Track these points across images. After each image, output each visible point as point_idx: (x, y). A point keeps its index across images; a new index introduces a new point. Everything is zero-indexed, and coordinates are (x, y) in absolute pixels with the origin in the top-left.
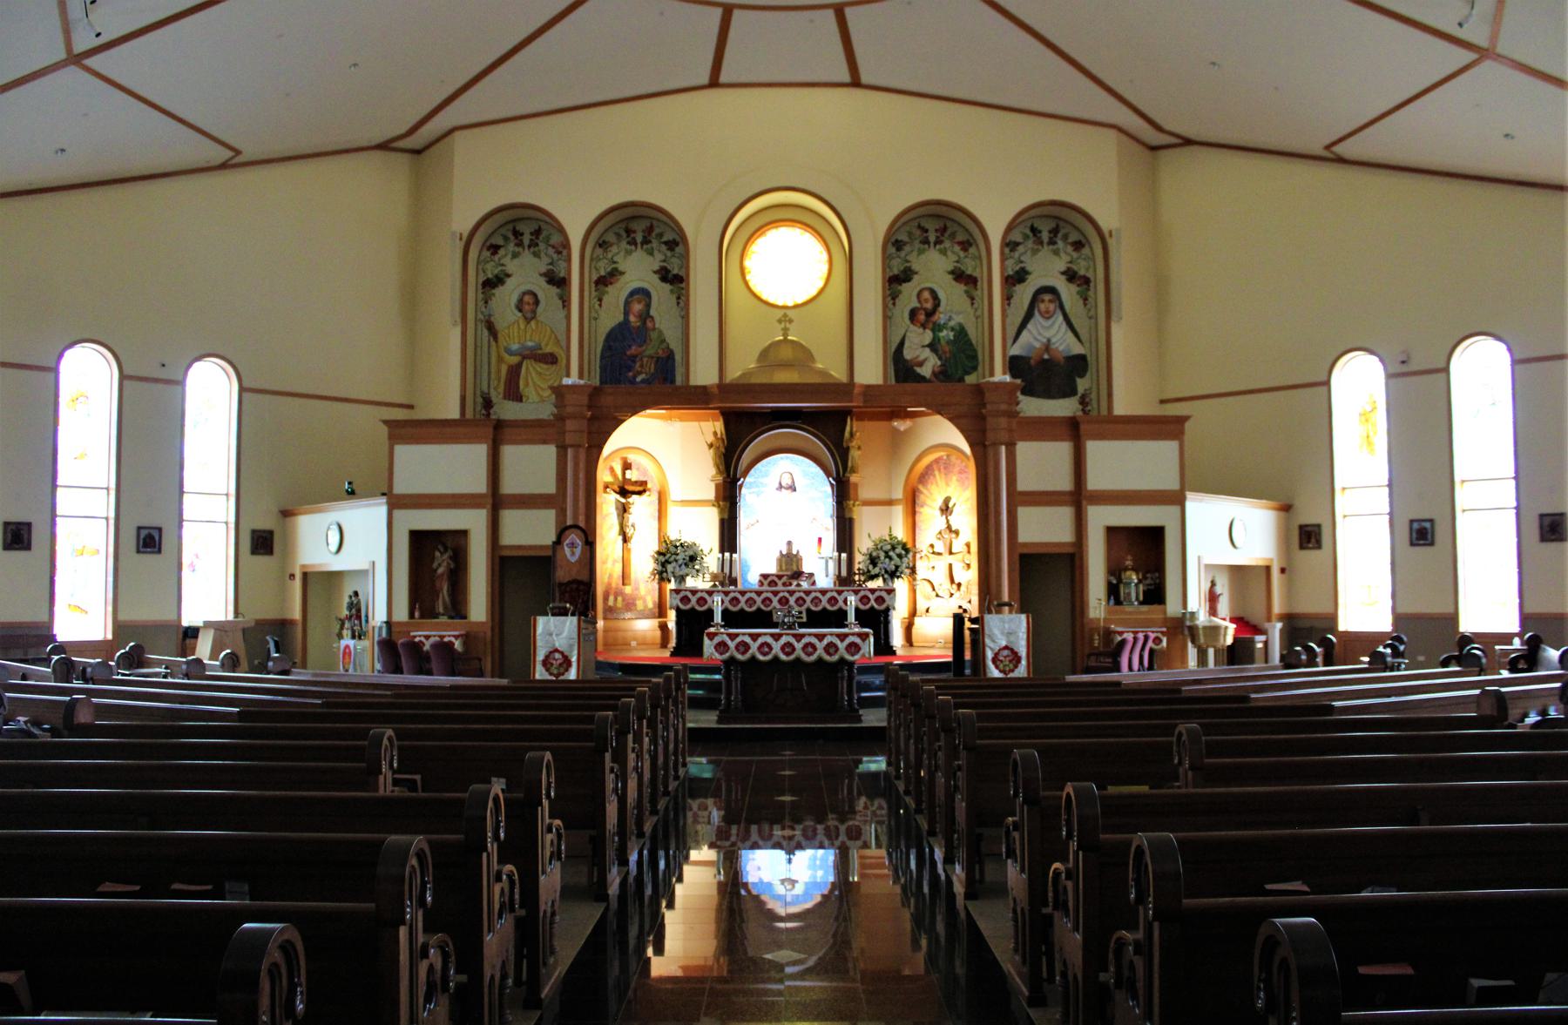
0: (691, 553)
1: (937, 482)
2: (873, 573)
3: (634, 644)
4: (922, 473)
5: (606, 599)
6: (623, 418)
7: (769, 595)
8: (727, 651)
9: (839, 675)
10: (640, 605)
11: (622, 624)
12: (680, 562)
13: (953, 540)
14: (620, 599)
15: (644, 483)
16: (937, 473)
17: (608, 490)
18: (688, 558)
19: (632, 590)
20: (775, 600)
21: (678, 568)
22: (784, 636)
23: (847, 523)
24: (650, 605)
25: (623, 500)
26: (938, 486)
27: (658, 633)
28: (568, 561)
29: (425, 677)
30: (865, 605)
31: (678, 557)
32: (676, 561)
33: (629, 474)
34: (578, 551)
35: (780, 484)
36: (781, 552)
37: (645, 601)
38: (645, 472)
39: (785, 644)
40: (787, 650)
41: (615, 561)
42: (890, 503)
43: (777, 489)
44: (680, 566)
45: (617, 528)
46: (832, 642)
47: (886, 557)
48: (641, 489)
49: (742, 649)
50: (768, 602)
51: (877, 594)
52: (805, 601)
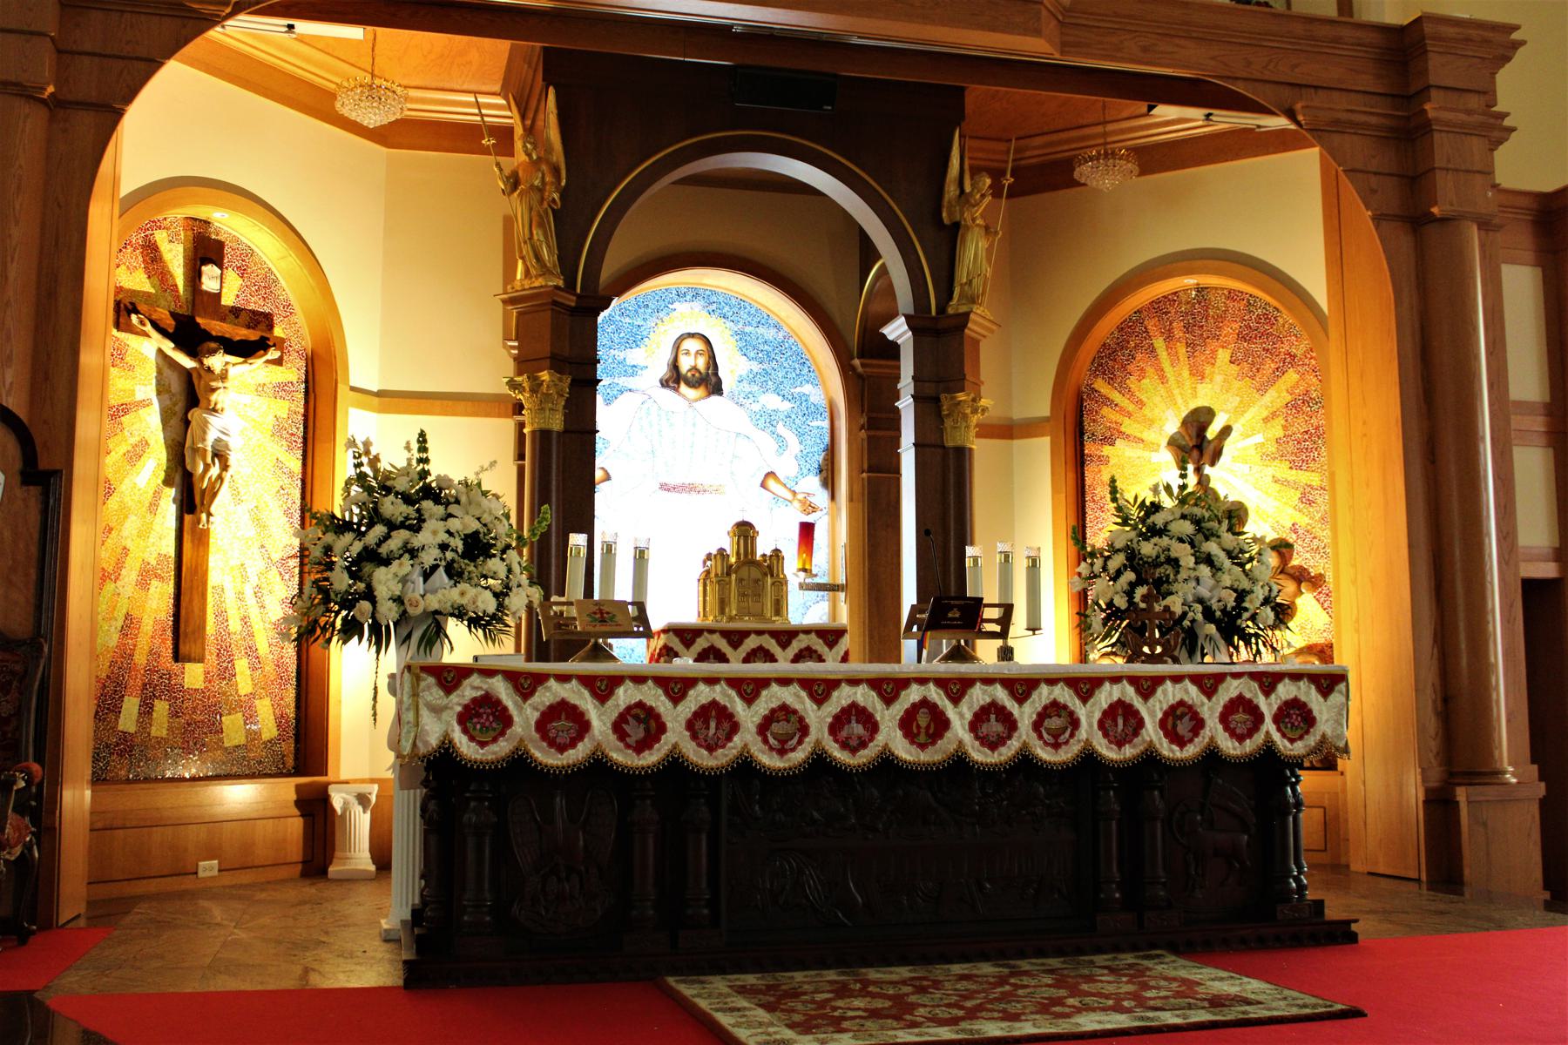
3: (208, 868)
5: (107, 706)
6: (209, 9)
7: (864, 696)
10: (233, 729)
11: (167, 800)
14: (161, 708)
15: (264, 320)
18: (458, 544)
19: (208, 678)
20: (888, 718)
24: (267, 726)
25: (187, 362)
26: (1163, 378)
27: (296, 825)
29: (1381, 250)
30: (1181, 742)
31: (418, 540)
32: (413, 553)
33: (210, 279)
35: (675, 366)
37: (250, 717)
38: (267, 284)
41: (147, 575)
44: (427, 575)
45: (157, 458)
48: (253, 335)
50: (857, 729)
51: (1285, 691)
52: (1011, 724)
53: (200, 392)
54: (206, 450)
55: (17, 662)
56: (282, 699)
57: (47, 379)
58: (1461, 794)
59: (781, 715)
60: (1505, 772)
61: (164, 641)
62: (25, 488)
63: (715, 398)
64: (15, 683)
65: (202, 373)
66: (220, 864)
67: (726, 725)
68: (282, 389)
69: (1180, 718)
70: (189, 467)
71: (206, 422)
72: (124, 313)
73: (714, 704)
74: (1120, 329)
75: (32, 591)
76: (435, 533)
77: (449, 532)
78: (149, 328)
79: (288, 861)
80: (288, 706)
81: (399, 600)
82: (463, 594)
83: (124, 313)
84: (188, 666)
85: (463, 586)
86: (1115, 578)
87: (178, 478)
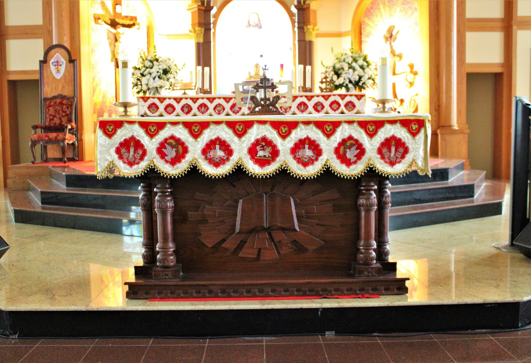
0: (165, 67)
1: (381, 15)
2: (337, 83)
4: (367, 9)
8: (142, 158)
9: (362, 201)
12: (153, 75)
13: (396, 62)
15: (134, 18)
16: (381, 7)
17: (100, 21)
18: (161, 71)
21: (152, 80)
22: (255, 126)
23: (308, 46)
28: (54, 78)
32: (150, 74)
34: (63, 69)
36: (250, 73)
39: (257, 143)
40: (261, 153)
42: (339, 35)
43: (246, 27)
44: (154, 79)
46: (350, 138)
47: (349, 68)
49: (171, 153)
58: (438, 132)
59: (219, 106)
60: (454, 126)
63: (260, 29)
67: (401, 150)
69: (319, 105)
72: (97, 20)
73: (203, 104)
74: (372, 3)
76: (156, 69)
77: (159, 69)
78: (103, 23)
81: (147, 85)
82: (162, 83)
83: (97, 20)
85: (162, 80)
87: (114, 60)
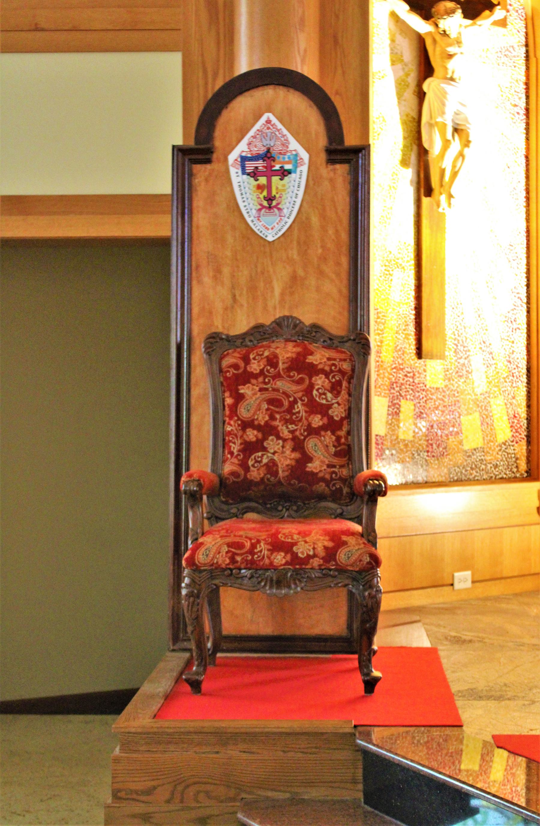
53: (435, 61)
54: (445, 125)
55: (345, 360)
56: (514, 398)
57: (336, 42)
61: (407, 337)
62: (331, 167)
64: (345, 384)
65: (438, 38)
66: (473, 575)
68: (506, 52)
70: (426, 145)
71: (444, 93)
75: (345, 282)
79: (533, 571)
80: (519, 405)
84: (429, 362)
86: (385, 270)
